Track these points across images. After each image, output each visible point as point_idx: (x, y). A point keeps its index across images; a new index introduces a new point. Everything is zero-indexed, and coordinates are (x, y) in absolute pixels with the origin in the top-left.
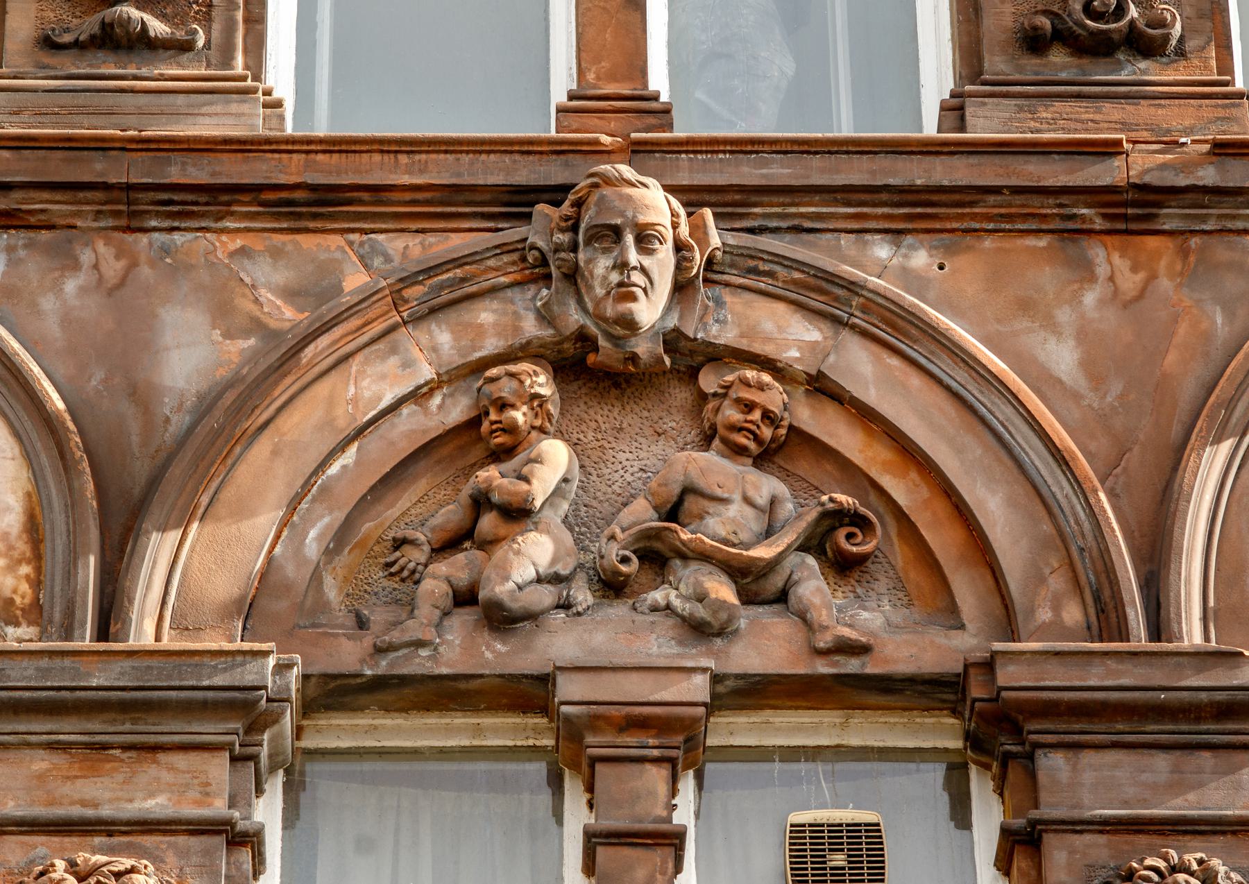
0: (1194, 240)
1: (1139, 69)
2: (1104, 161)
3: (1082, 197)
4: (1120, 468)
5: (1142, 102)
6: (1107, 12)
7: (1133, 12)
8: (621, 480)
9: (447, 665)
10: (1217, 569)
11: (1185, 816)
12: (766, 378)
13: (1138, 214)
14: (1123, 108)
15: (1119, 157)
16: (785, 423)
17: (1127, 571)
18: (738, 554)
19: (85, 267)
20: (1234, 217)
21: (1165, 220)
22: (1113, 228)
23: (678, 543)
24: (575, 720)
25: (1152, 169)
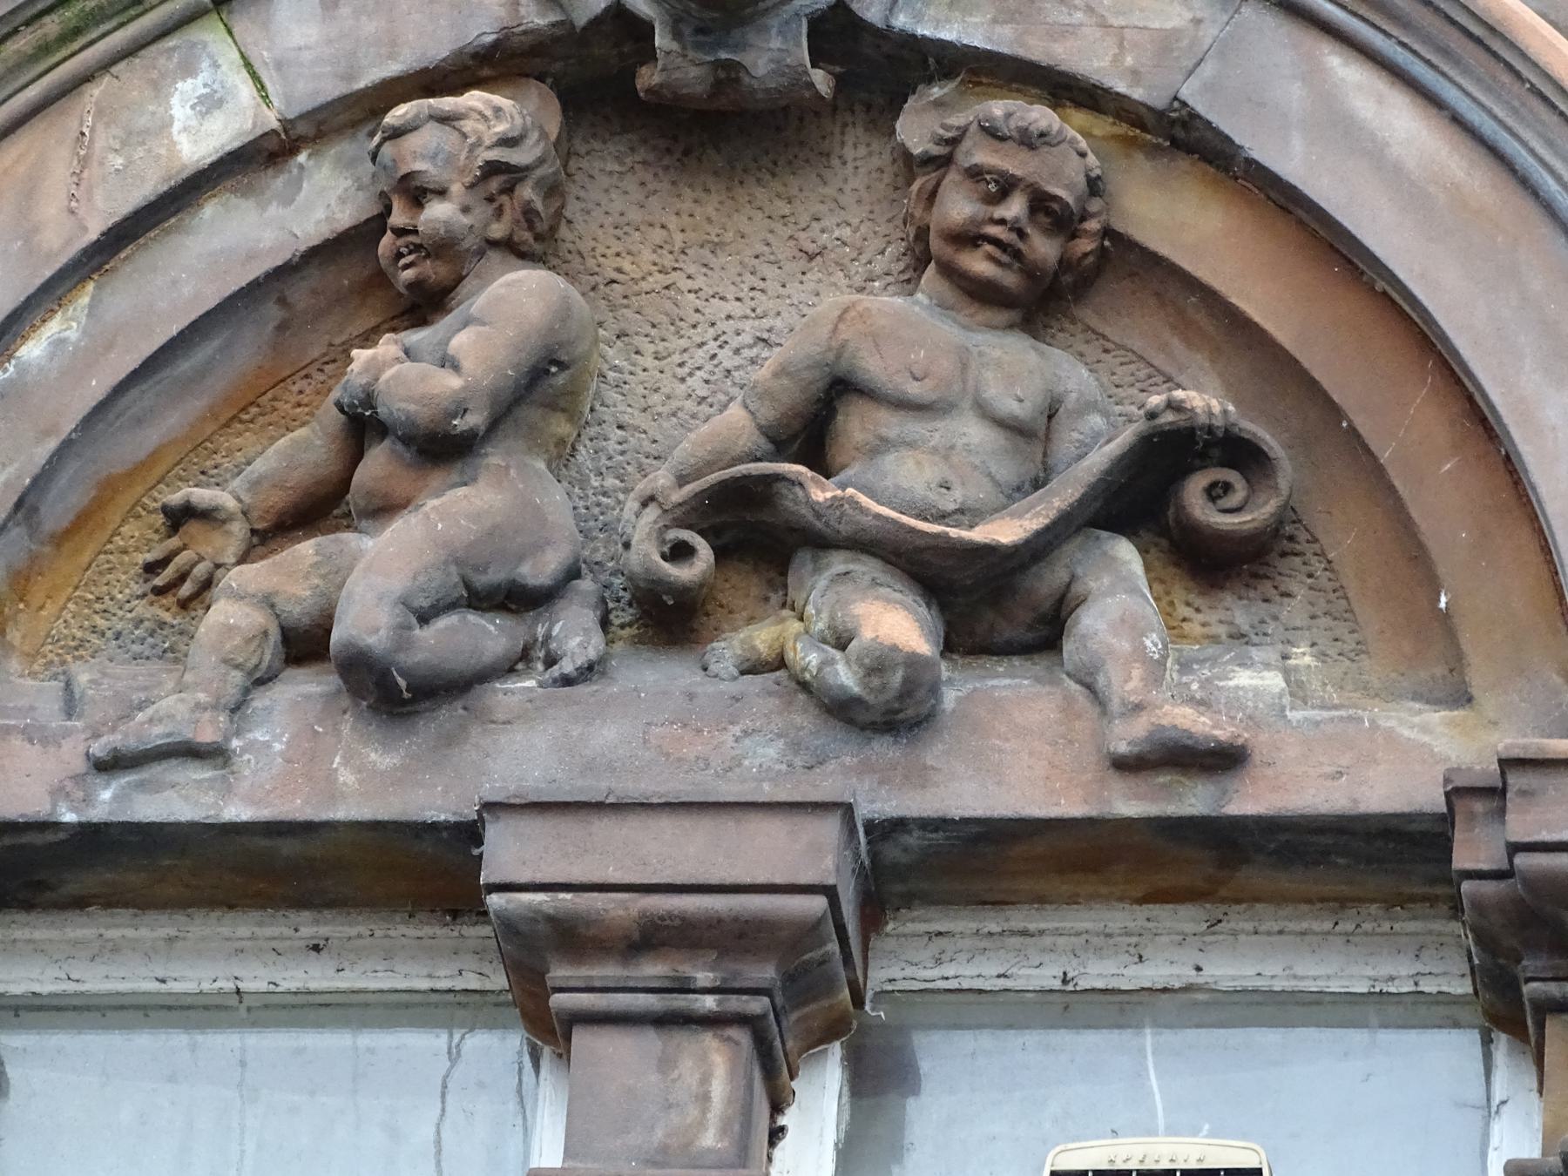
8: (709, 367)
9: (250, 800)
12: (1041, 116)
16: (1093, 225)
18: (937, 536)
23: (804, 511)
24: (523, 928)
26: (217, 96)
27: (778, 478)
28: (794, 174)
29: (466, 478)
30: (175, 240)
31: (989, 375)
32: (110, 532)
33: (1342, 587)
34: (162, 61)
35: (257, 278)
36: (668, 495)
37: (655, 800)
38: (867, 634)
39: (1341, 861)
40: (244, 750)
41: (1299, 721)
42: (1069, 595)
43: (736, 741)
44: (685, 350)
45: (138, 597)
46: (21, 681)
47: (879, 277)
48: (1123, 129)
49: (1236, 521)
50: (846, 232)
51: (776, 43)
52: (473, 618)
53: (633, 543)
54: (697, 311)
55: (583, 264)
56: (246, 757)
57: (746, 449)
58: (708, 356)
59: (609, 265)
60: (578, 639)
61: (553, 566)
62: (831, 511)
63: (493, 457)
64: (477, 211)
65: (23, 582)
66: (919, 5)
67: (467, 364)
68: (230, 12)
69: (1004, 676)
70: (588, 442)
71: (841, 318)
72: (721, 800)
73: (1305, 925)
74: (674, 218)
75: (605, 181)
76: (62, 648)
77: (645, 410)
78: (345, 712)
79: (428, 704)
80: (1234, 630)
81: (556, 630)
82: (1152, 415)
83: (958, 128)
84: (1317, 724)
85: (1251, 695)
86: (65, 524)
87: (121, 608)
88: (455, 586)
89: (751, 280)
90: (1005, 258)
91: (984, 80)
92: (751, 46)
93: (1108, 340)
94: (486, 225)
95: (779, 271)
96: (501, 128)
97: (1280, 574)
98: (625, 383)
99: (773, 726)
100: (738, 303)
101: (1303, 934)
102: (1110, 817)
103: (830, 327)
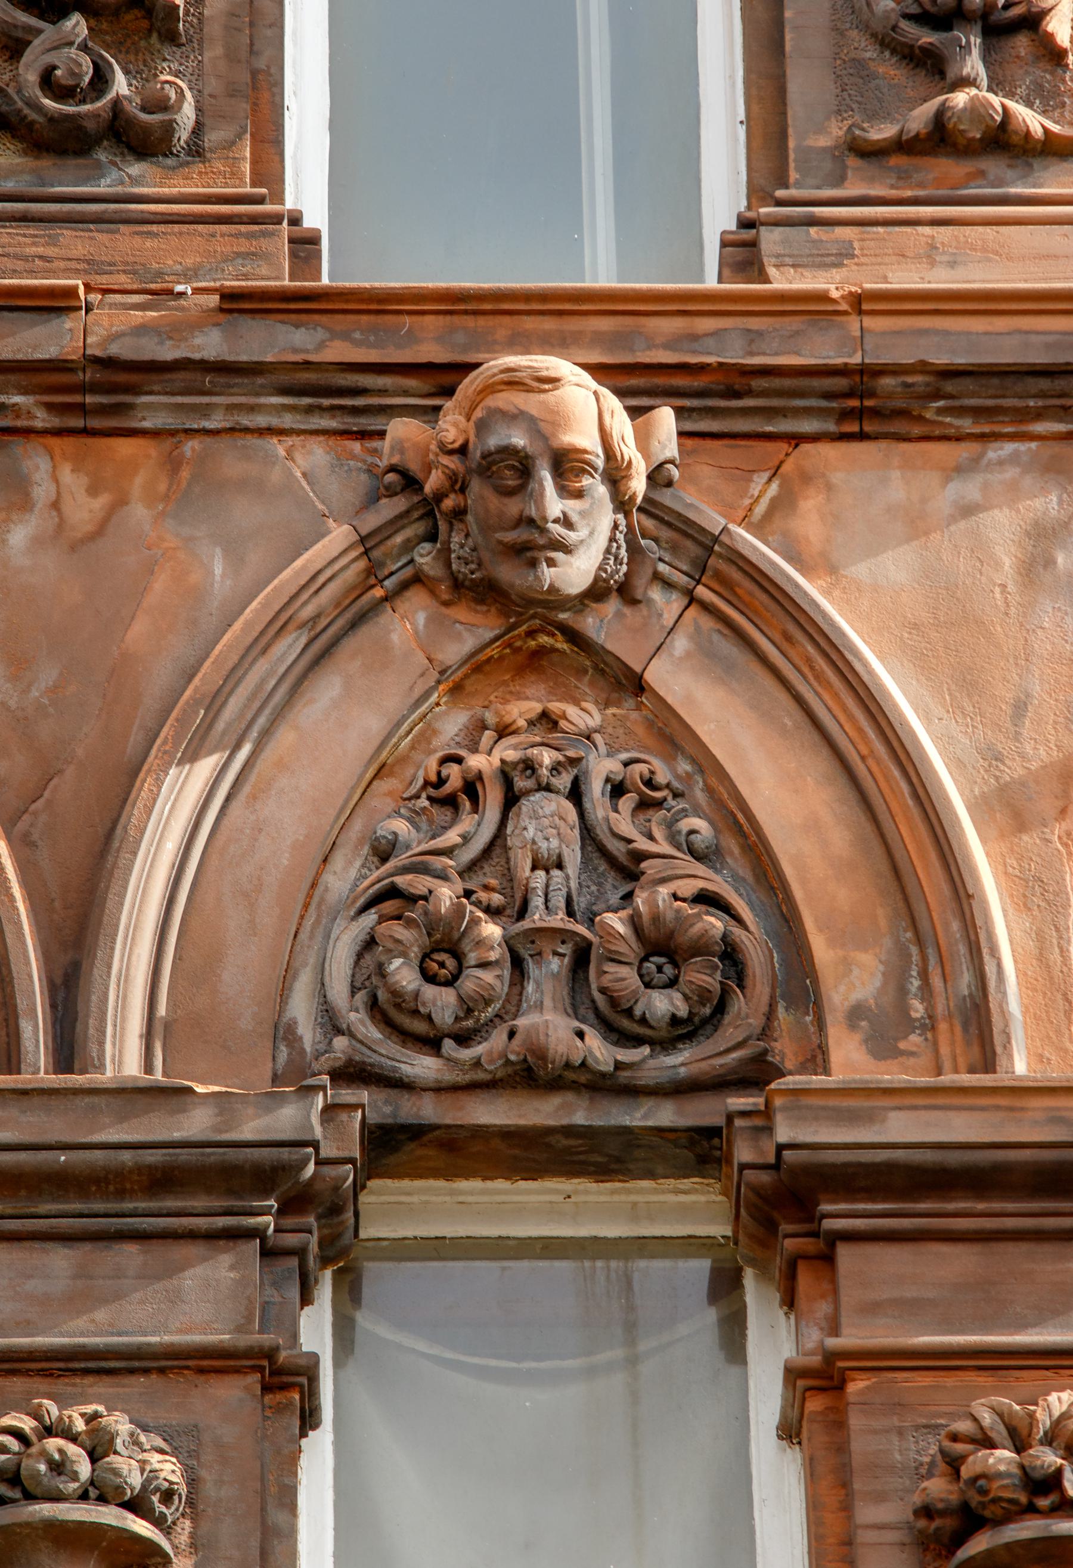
0: (190, 444)
1: (129, 176)
2: (49, 320)
3: (13, 378)
4: (41, 801)
5: (122, 227)
6: (78, 85)
7: (121, 85)
10: (178, 958)
11: (84, 1346)
13: (101, 404)
14: (91, 238)
15: (72, 315)
17: (28, 963)
19: (39, 505)
20: (252, 409)
21: (145, 414)
22: (64, 425)
25: (123, 334)
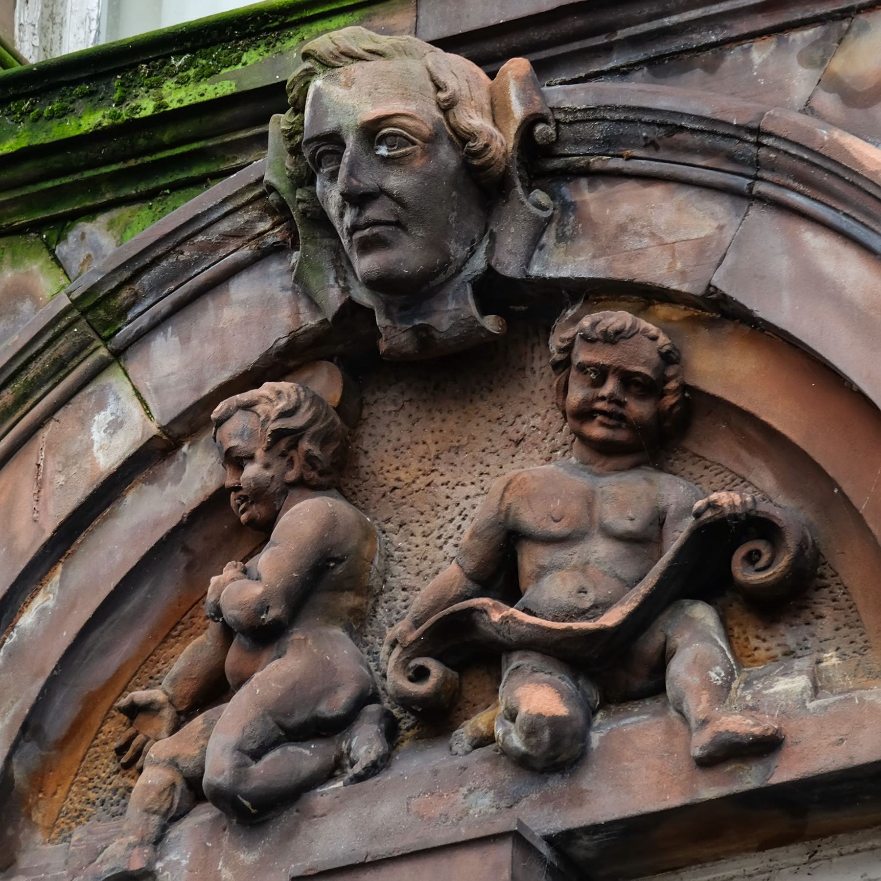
8: (457, 535)
16: (672, 385)
26: (120, 419)
27: (472, 610)
28: (503, 387)
29: (280, 653)
30: (110, 523)
31: (607, 507)
32: (95, 732)
33: (854, 604)
34: (85, 403)
35: (162, 538)
36: (405, 637)
37: (396, 854)
38: (523, 710)
39: (867, 798)
40: (164, 869)
41: (814, 709)
42: (667, 651)
43: (465, 798)
44: (442, 527)
45: (115, 773)
46: (44, 847)
47: (559, 448)
48: (691, 312)
49: (764, 576)
50: (537, 421)
51: (452, 306)
52: (291, 748)
53: (387, 674)
54: (448, 497)
55: (376, 480)
56: (166, 873)
57: (458, 593)
58: (456, 527)
59: (391, 476)
60: (365, 748)
61: (344, 701)
62: (503, 627)
63: (297, 635)
64: (275, 466)
65: (39, 779)
66: (546, 257)
67: (265, 576)
68: (125, 360)
69: (638, 714)
70: (384, 605)
71: (506, 489)
72: (430, 846)
73: (870, 843)
74: (430, 435)
75: (386, 419)
76: (69, 819)
77: (418, 574)
78: (225, 830)
79: (273, 813)
80: (787, 649)
81: (354, 743)
82: (697, 515)
83: (569, 339)
84: (825, 708)
85: (783, 696)
86: (64, 732)
87: (104, 783)
88: (273, 730)
89: (480, 468)
90: (612, 422)
91: (603, 297)
92: (435, 311)
93: (706, 460)
94: (284, 473)
95: (497, 457)
96: (281, 405)
97: (815, 603)
98: (405, 558)
99: (486, 783)
100: (473, 486)
101: (872, 849)
102: (698, 801)
103: (499, 497)
